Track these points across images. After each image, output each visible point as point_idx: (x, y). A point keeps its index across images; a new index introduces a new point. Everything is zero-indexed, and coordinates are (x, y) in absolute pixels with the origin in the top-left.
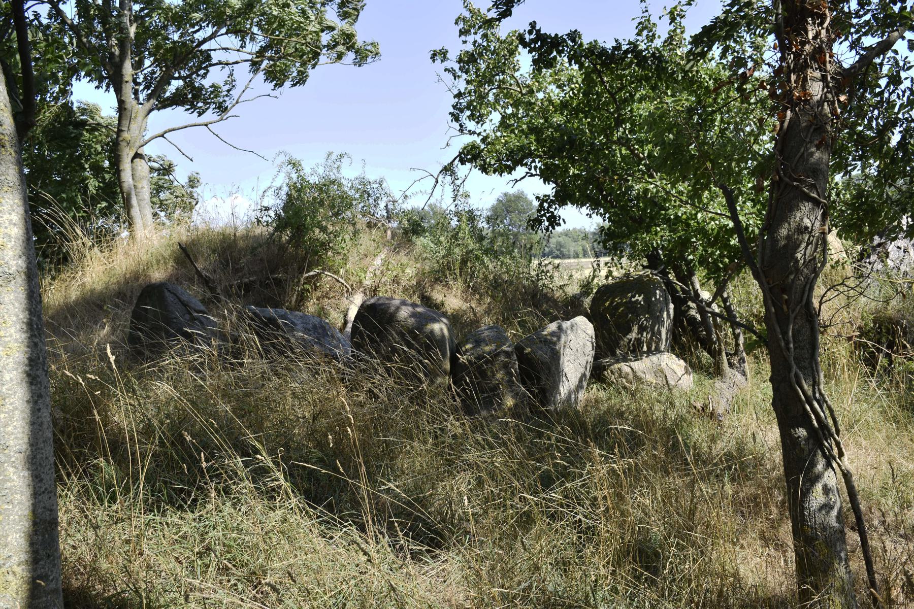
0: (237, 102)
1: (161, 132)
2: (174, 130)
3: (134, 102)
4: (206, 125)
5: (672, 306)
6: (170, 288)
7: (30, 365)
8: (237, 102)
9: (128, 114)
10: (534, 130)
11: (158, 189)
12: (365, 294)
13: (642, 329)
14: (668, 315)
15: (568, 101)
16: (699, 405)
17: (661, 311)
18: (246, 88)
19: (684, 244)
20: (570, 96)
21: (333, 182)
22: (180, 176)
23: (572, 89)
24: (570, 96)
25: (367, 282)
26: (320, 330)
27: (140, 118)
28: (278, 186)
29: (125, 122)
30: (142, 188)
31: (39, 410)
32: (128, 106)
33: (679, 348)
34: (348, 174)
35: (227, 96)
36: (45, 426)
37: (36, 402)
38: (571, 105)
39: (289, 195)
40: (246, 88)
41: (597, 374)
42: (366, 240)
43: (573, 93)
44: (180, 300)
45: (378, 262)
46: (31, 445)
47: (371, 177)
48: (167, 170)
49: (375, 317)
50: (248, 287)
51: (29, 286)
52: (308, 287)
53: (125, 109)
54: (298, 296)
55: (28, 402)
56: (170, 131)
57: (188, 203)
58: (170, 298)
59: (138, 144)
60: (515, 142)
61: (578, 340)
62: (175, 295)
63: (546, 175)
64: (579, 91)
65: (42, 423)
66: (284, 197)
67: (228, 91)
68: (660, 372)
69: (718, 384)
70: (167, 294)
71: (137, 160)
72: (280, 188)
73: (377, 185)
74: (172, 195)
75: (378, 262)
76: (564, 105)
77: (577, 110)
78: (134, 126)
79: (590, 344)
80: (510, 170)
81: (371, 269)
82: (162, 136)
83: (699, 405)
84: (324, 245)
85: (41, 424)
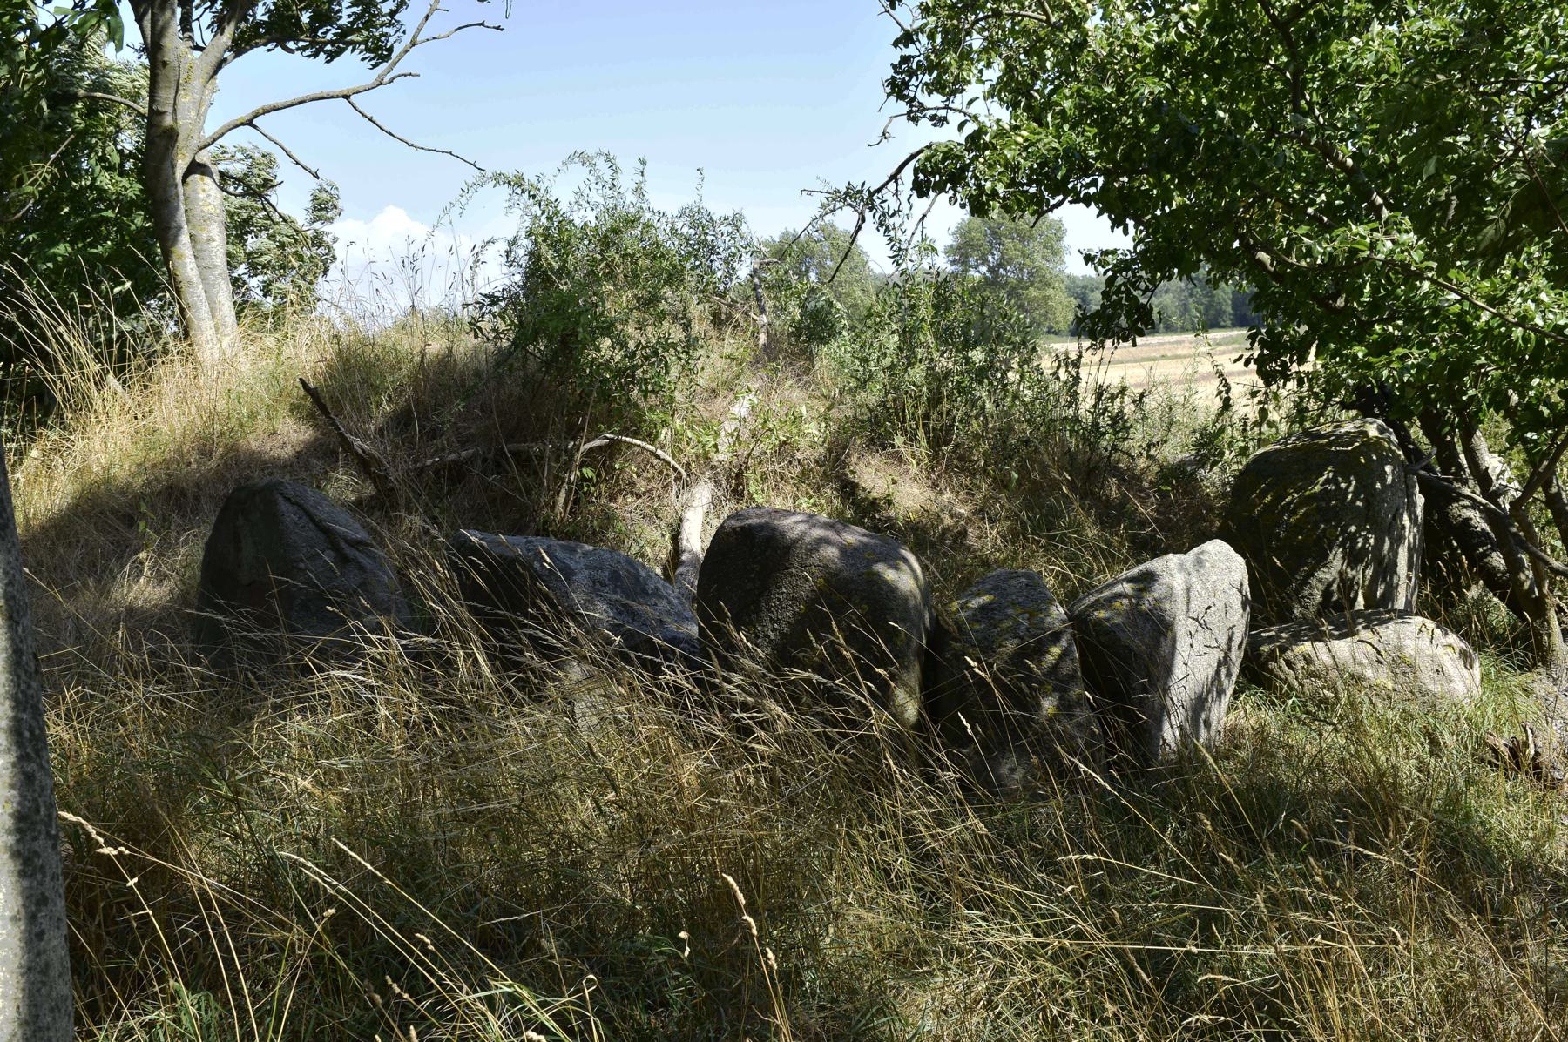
0: (413, 44)
1: (244, 113)
2: (275, 109)
3: (184, 46)
4: (346, 97)
5: (1420, 500)
6: (290, 492)
7: (19, 830)
8: (413, 44)
9: (172, 75)
10: (1091, 111)
11: (239, 228)
12: (717, 483)
13: (1354, 558)
14: (1412, 514)
15: (1172, 44)
16: (1501, 743)
17: (1397, 516)
18: (433, 9)
19: (1462, 366)
20: (1178, 34)
21: (632, 221)
22: (291, 201)
23: (1184, 17)
24: (1178, 34)
25: (723, 456)
26: (626, 583)
27: (197, 83)
28: (510, 237)
29: (165, 95)
30: (210, 240)
31: (40, 935)
32: (169, 56)
33: (1441, 605)
34: (666, 201)
35: (390, 25)
36: (54, 973)
37: (32, 919)
38: (1180, 52)
39: (534, 255)
40: (433, 9)
41: (1256, 672)
42: (712, 362)
43: (1186, 26)
44: (312, 520)
45: (741, 408)
46: (24, 1023)
47: (719, 209)
48: (256, 188)
49: (747, 555)
50: (456, 473)
51: (11, 639)
52: (588, 472)
53: (165, 64)
54: (569, 492)
55: (14, 919)
56: (266, 111)
57: (307, 256)
58: (290, 515)
59: (195, 143)
60: (1049, 142)
61: (1206, 587)
62: (301, 507)
63: (1117, 207)
64: (1200, 22)
65: (47, 965)
66: (524, 261)
67: (393, 13)
68: (1401, 664)
69: (1540, 683)
70: (284, 506)
71: (195, 178)
72: (513, 243)
73: (729, 229)
74: (283, 258)
75: (741, 408)
76: (1165, 54)
77: (1193, 66)
78: (185, 100)
79: (1237, 601)
80: (1105, 295)
81: (729, 426)
82: (250, 123)
83: (1501, 743)
84: (626, 374)
85: (45, 971)
